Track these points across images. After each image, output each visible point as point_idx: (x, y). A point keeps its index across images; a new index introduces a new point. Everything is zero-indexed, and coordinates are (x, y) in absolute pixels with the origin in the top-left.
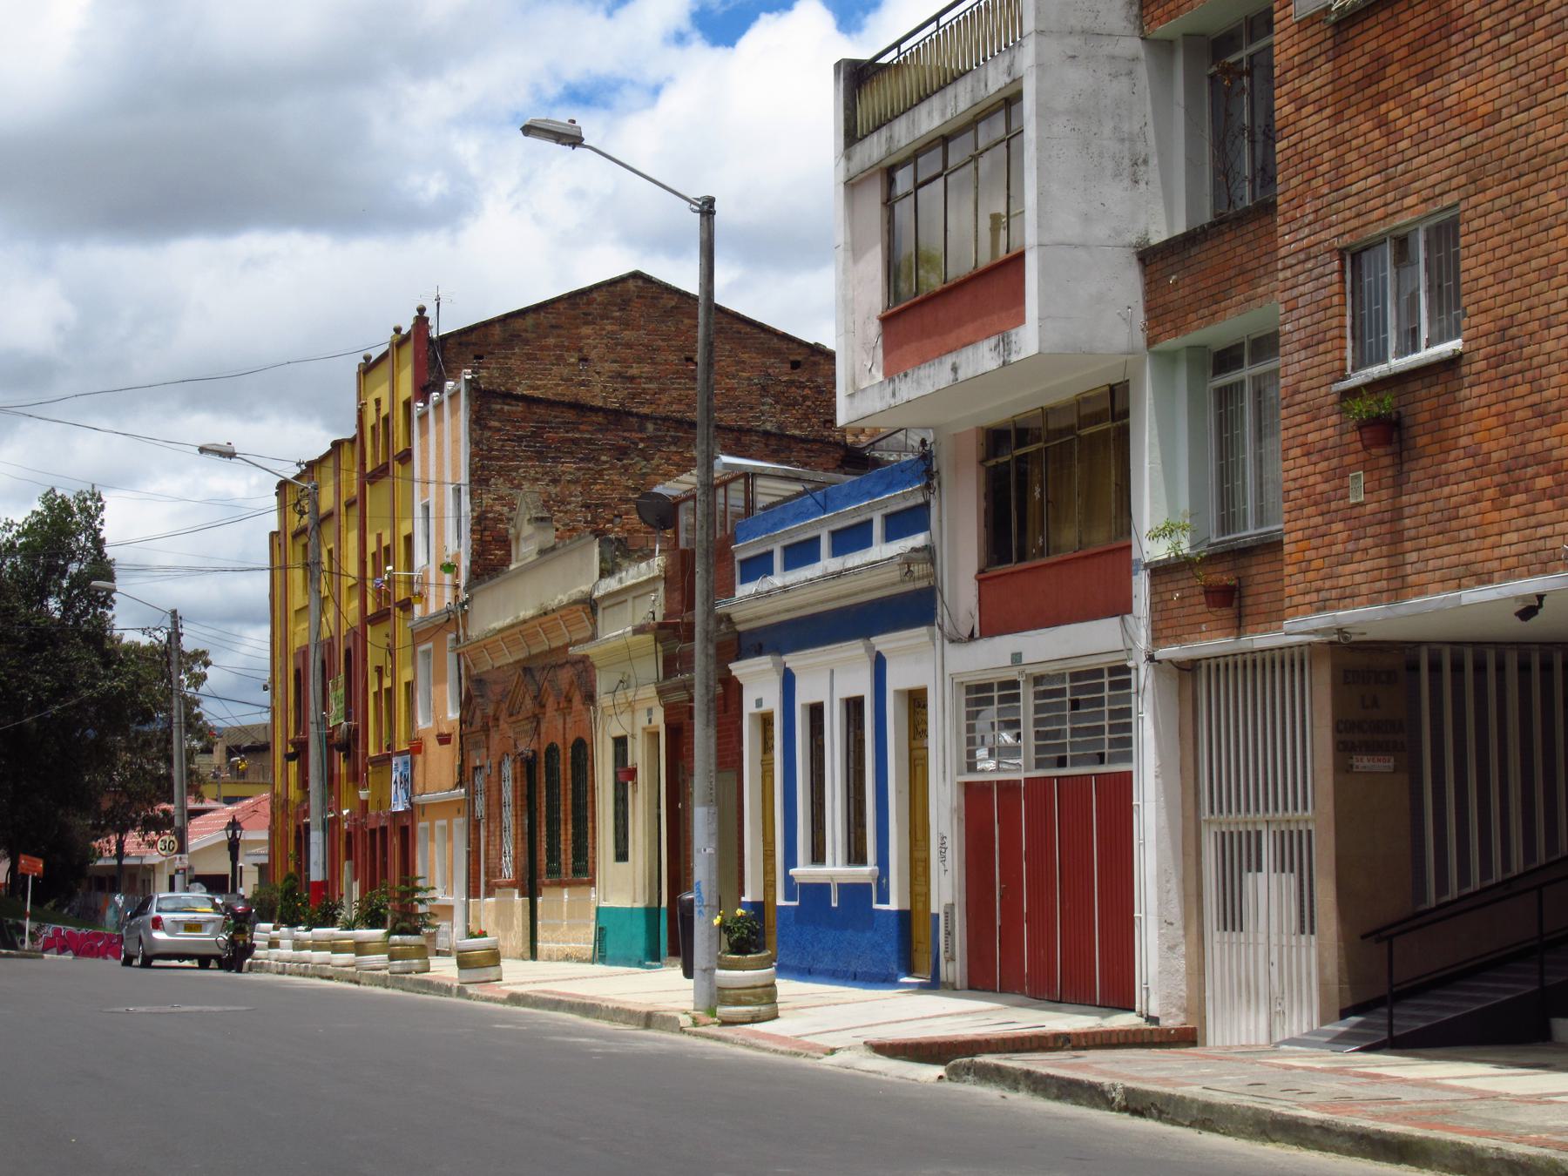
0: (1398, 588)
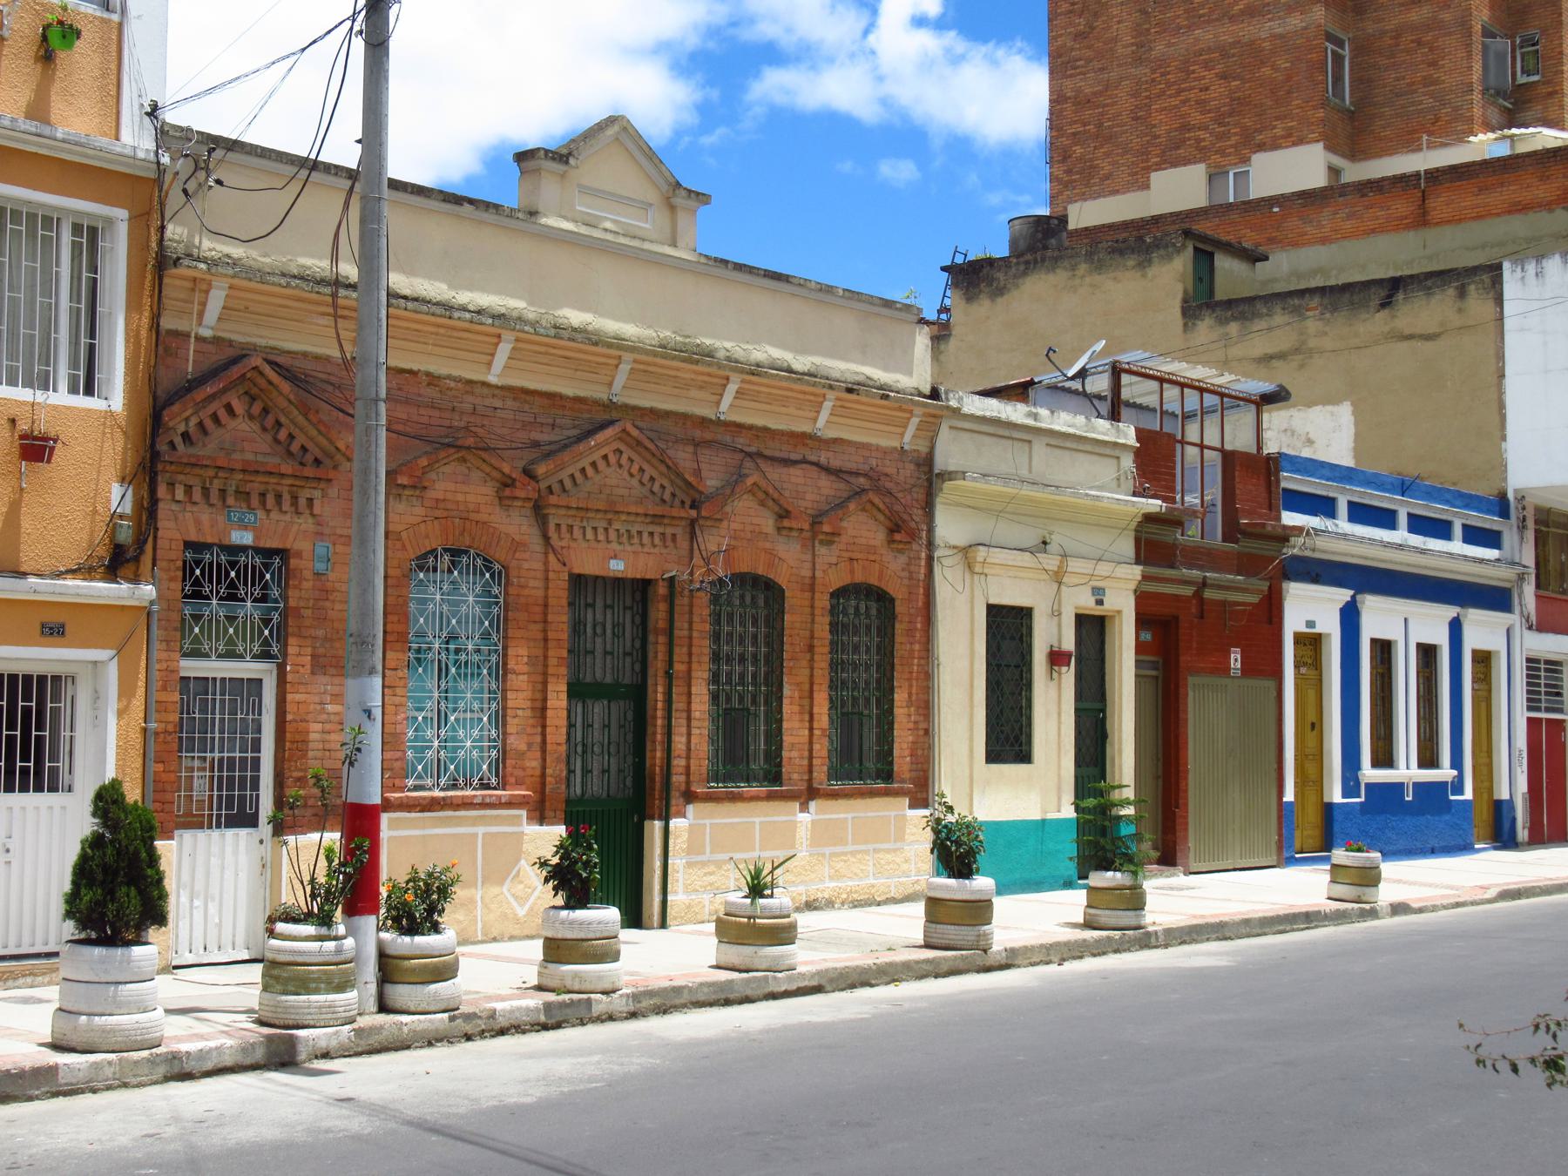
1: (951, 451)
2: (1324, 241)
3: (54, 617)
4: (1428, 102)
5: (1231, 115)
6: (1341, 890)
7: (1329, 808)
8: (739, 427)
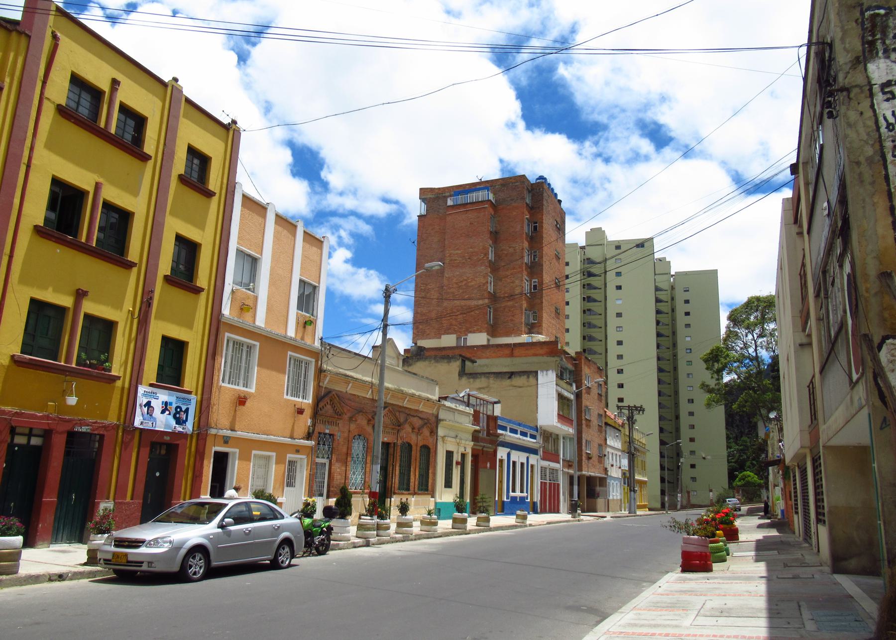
0: (588, 472)
1: (442, 415)
2: (487, 358)
3: (297, 448)
4: (512, 325)
5: (463, 323)
6: (519, 520)
7: (503, 502)
8: (406, 408)
